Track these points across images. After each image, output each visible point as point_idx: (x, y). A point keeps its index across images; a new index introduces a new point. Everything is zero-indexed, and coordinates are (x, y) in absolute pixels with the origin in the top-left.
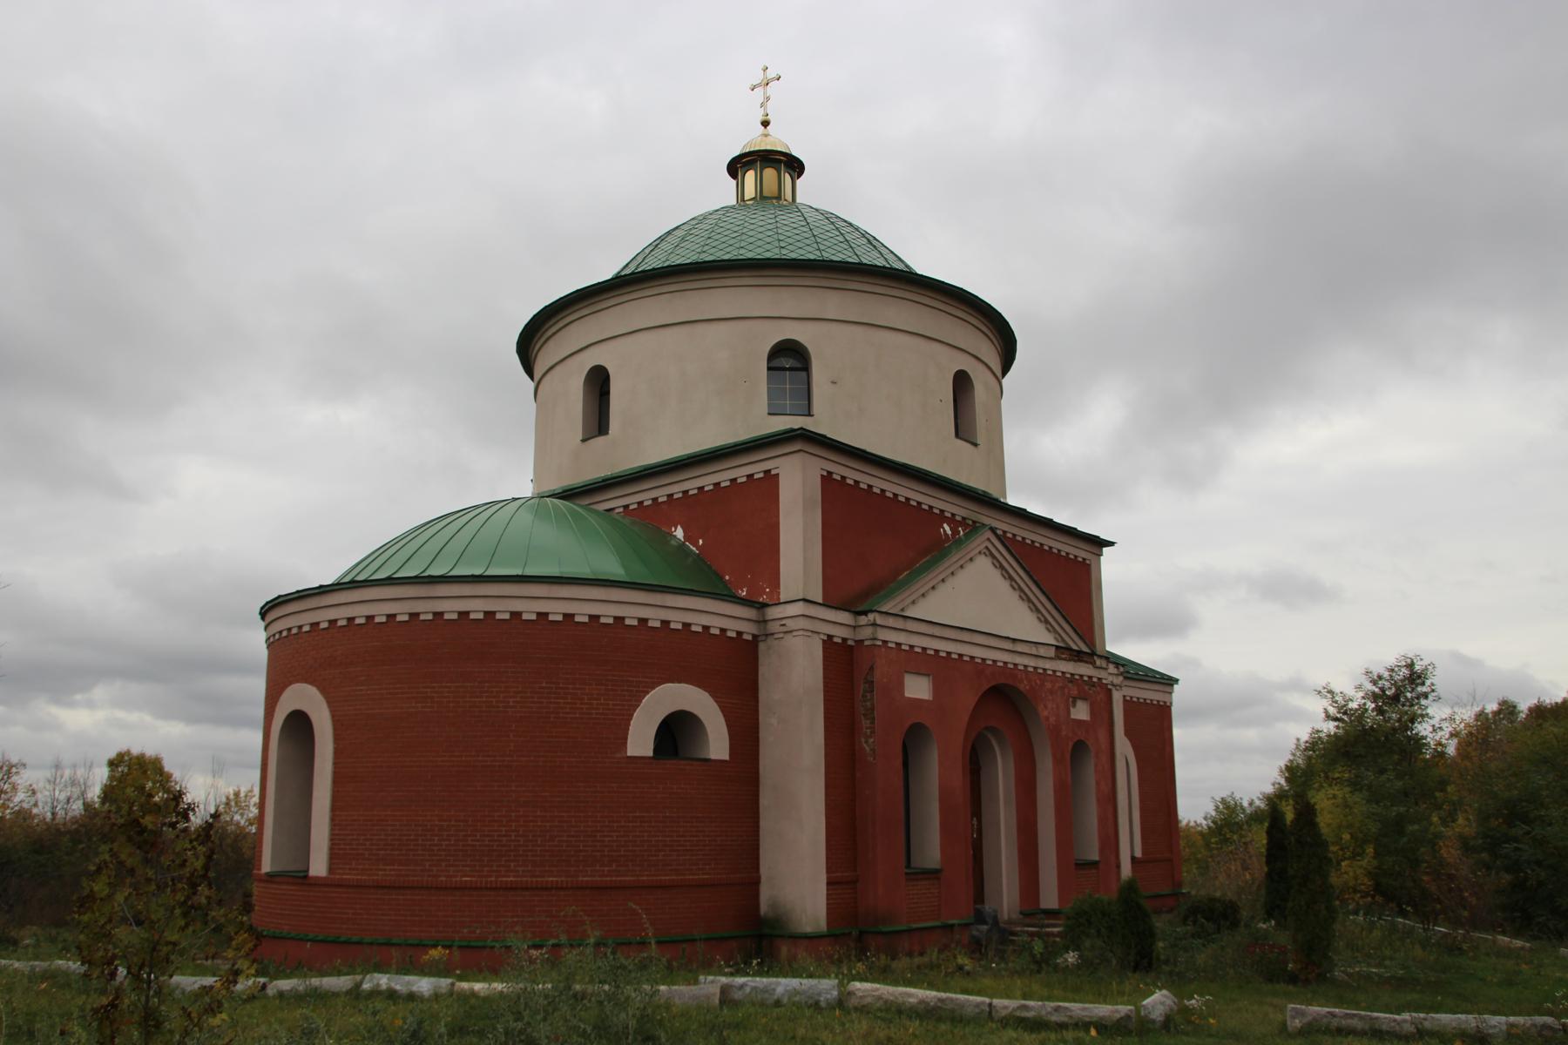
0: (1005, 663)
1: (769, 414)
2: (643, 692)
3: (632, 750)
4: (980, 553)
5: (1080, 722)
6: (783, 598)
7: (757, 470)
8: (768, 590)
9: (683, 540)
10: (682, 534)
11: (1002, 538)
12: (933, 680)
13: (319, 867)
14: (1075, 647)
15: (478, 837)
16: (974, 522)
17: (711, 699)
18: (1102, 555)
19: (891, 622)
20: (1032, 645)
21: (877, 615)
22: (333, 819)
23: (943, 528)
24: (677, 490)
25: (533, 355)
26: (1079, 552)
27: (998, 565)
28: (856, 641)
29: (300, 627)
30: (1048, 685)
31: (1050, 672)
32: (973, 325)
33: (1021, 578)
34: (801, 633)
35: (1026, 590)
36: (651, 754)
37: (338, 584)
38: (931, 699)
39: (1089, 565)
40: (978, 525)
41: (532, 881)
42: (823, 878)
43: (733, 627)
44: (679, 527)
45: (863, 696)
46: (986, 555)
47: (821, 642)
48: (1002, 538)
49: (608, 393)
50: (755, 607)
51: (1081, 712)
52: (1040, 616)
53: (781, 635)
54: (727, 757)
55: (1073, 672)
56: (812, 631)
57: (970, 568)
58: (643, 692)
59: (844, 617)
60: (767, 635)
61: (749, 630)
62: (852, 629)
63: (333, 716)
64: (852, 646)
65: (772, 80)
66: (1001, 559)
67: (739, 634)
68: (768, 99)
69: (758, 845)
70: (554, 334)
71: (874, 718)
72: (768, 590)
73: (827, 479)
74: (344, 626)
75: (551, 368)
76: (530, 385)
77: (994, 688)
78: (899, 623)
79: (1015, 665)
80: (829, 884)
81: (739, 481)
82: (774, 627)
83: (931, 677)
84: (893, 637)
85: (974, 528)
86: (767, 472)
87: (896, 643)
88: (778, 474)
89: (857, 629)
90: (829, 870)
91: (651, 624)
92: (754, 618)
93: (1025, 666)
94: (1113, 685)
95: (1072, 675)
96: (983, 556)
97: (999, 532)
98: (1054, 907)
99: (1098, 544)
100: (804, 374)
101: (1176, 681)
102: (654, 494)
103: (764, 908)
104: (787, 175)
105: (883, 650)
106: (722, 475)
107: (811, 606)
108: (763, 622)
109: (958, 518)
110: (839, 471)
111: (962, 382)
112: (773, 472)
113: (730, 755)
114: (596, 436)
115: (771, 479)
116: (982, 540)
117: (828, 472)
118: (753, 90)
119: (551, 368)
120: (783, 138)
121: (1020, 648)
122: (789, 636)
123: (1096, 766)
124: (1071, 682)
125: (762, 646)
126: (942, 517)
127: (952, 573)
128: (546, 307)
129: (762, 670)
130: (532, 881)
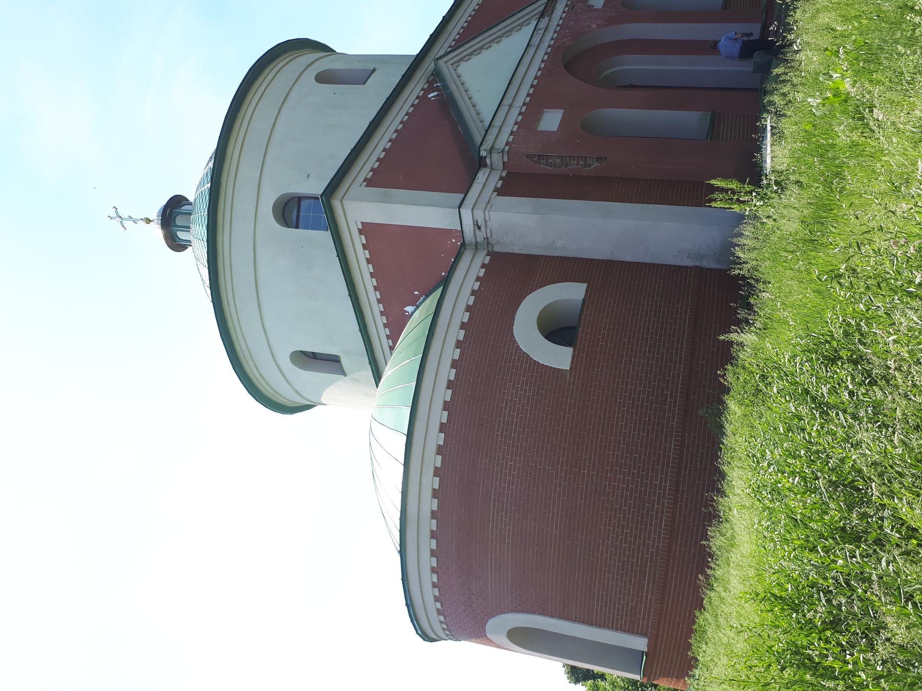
0: (546, 53)
2: (516, 352)
4: (455, 70)
9: (415, 307)
13: (640, 643)
14: (543, 7)
16: (432, 75)
19: (491, 138)
21: (482, 148)
22: (599, 626)
23: (432, 97)
24: (378, 308)
28: (504, 169)
29: (441, 622)
31: (561, 22)
34: (487, 212)
36: (569, 351)
40: (434, 73)
41: (672, 467)
44: (405, 309)
45: (551, 166)
46: (459, 65)
49: (313, 353)
50: (464, 251)
52: (515, 29)
54: (585, 285)
55: (565, 5)
56: (488, 204)
57: (465, 78)
59: (482, 176)
60: (488, 244)
61: (482, 258)
62: (493, 171)
63: (512, 611)
65: (117, 213)
67: (483, 266)
69: (666, 265)
70: (272, 388)
72: (454, 240)
73: (369, 183)
74: (439, 591)
75: (297, 392)
76: (319, 407)
77: (565, 67)
78: (494, 131)
79: (549, 46)
81: (368, 256)
82: (481, 235)
84: (505, 137)
85: (437, 75)
89: (493, 167)
91: (461, 338)
92: (473, 253)
93: (552, 39)
95: (566, 6)
98: (760, 28)
100: (304, 203)
102: (381, 326)
104: (182, 208)
107: (465, 202)
108: (477, 246)
109: (426, 87)
110: (366, 173)
111: (324, 78)
112: (360, 227)
115: (367, 229)
116: (445, 67)
117: (364, 181)
119: (297, 392)
120: (154, 209)
122: (489, 223)
126: (422, 99)
127: (466, 91)
129: (516, 250)
130: (672, 467)
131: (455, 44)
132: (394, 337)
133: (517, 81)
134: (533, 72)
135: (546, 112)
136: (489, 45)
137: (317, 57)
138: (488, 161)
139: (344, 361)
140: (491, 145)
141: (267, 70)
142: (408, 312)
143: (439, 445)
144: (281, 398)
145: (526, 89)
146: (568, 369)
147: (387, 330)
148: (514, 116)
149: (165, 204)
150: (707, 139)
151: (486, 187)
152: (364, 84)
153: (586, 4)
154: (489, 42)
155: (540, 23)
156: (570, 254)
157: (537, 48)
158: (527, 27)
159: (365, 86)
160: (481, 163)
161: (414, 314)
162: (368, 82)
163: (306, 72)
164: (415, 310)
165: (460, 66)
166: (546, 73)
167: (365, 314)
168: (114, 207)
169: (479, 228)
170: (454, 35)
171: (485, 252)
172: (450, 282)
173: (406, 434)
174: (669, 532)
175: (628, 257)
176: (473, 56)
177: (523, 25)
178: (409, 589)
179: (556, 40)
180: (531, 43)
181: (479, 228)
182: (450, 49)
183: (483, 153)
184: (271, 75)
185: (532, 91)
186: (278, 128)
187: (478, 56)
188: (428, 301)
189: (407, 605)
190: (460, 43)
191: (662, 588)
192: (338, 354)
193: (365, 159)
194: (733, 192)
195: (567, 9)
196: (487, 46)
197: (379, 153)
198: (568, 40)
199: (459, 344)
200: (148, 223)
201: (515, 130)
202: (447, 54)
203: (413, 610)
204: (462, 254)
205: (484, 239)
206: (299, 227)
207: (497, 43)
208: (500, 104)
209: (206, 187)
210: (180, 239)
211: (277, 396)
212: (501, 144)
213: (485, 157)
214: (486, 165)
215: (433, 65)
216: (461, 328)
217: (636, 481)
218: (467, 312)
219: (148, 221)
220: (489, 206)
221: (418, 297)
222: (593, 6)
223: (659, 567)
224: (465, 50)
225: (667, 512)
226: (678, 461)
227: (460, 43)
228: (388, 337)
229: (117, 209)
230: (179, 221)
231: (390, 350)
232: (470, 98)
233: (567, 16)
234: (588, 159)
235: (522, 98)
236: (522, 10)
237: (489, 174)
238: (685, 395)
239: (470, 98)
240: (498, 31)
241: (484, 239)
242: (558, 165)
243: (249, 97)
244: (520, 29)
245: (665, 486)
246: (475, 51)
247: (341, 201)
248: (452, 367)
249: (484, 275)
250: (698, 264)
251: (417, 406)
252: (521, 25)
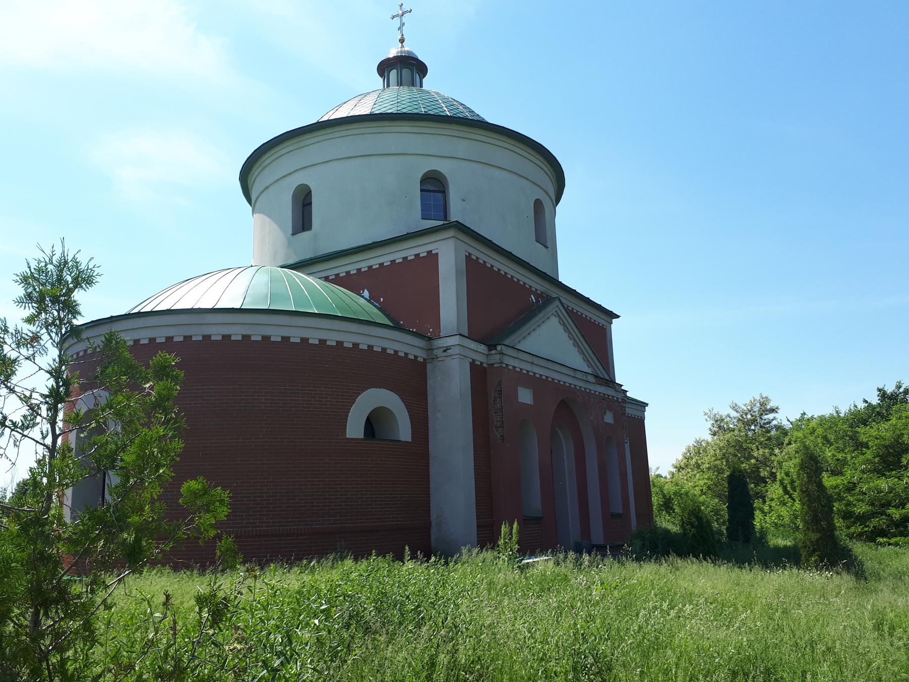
1: (422, 219)
2: (358, 393)
3: (349, 434)
4: (552, 314)
6: (442, 334)
7: (422, 251)
8: (431, 330)
10: (368, 295)
14: (601, 376)
16: (547, 296)
17: (400, 400)
21: (503, 346)
24: (364, 266)
25: (251, 186)
31: (593, 392)
32: (545, 171)
34: (458, 356)
35: (577, 340)
36: (362, 436)
37: (129, 314)
39: (606, 329)
43: (412, 353)
44: (366, 290)
45: (494, 401)
46: (556, 316)
47: (469, 363)
49: (310, 204)
51: (609, 418)
53: (443, 358)
54: (411, 441)
58: (358, 393)
59: (482, 348)
61: (422, 355)
64: (486, 368)
65: (407, 12)
66: (564, 320)
67: (416, 357)
68: (403, 24)
70: (269, 164)
72: (431, 330)
73: (468, 257)
75: (267, 188)
76: (250, 208)
80: (478, 526)
82: (439, 352)
83: (532, 390)
84: (511, 362)
85: (547, 300)
86: (429, 252)
87: (513, 367)
88: (438, 253)
89: (489, 356)
92: (425, 348)
96: (554, 316)
99: (613, 316)
100: (440, 195)
101: (647, 404)
104: (417, 74)
106: (396, 254)
108: (430, 350)
109: (539, 292)
110: (475, 254)
111: (538, 204)
114: (301, 232)
115: (432, 257)
117: (469, 253)
118: (392, 19)
119: (267, 188)
121: (579, 375)
125: (429, 366)
126: (529, 291)
128: (264, 144)
129: (430, 382)
132: (337, 280)
133: (550, 365)
134: (557, 377)
135: (531, 391)
137: (551, 195)
138: (494, 352)
139: (306, 235)
140: (506, 353)
141: (541, 159)
142: (363, 293)
143: (270, 337)
144: (258, 171)
145: (545, 373)
146: (347, 437)
147: (344, 274)
148: (526, 367)
149: (419, 59)
150: (524, 516)
152: (536, 241)
154: (587, 359)
155: (591, 376)
156: (430, 425)
157: (574, 377)
159: (535, 241)
160: (492, 347)
161: (362, 298)
162: (538, 244)
163: (542, 190)
164: (366, 299)
166: (556, 386)
167: (358, 255)
168: (411, 10)
169: (445, 351)
170: (576, 308)
171: (426, 357)
172: (402, 332)
173: (270, 308)
175: (433, 471)
176: (563, 327)
177: (587, 362)
178: (129, 318)
179: (580, 390)
180: (577, 371)
181: (445, 351)
182: (566, 306)
183: (499, 348)
184: (540, 164)
185: (544, 378)
186: (497, 172)
187: (559, 323)
188: (376, 310)
189: (112, 317)
190: (571, 313)
192: (313, 229)
193: (484, 252)
194: (510, 539)
195: (602, 395)
196: (571, 337)
197: (490, 262)
198: (581, 399)
199: (356, 345)
200: (400, 41)
201: (517, 369)
203: (103, 323)
204: (422, 339)
205: (437, 356)
206: (423, 193)
207: (574, 344)
208: (533, 355)
209: (445, 108)
210: (390, 72)
211: (260, 168)
212: (508, 361)
213: (497, 350)
214: (490, 350)
215: (554, 296)
216: (369, 346)
219: (402, 41)
220: (462, 357)
221: (378, 301)
222: (605, 414)
224: (567, 320)
227: (571, 313)
228: (337, 275)
229: (410, 12)
230: (406, 72)
231: (325, 277)
232: (534, 330)
234: (502, 429)
235: (539, 371)
236: (598, 360)
237: (484, 354)
239: (534, 330)
240: (582, 343)
241: (437, 356)
242: (495, 406)
243: (521, 146)
244: (584, 360)
245: (262, 527)
246: (567, 328)
247: (453, 237)
248: (337, 342)
249: (409, 359)
250: (433, 524)
251: (305, 316)
252: (588, 361)
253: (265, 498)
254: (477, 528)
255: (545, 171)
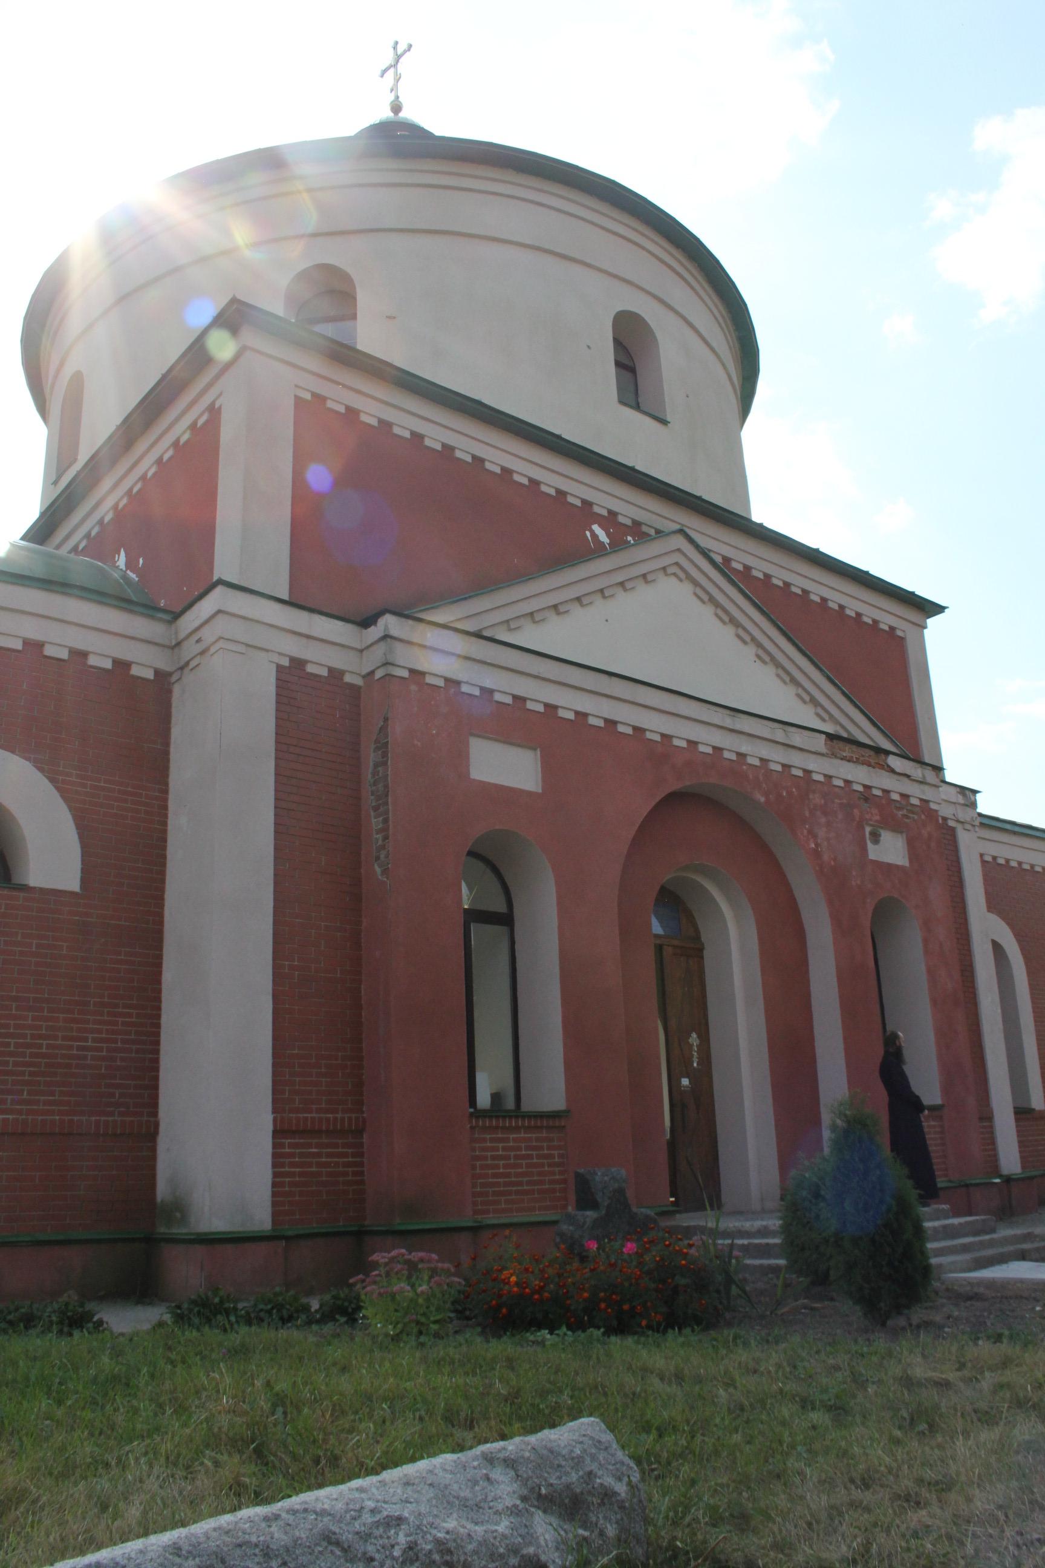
5: (888, 869)
11: (724, 567)
12: (542, 757)
15: (25, 1096)
18: (925, 627)
20: (776, 725)
26: (886, 615)
27: (705, 598)
30: (816, 799)
32: (650, 252)
33: (732, 601)
38: (540, 791)
39: (902, 639)
42: (266, 1121)
47: (274, 668)
48: (724, 567)
50: (160, 620)
52: (800, 691)
56: (247, 645)
57: (644, 594)
60: (182, 668)
64: (360, 687)
69: (156, 1061)
71: (387, 812)
73: (296, 397)
80: (279, 1133)
83: (538, 752)
90: (278, 1104)
94: (958, 821)
97: (718, 559)
99: (929, 609)
103: (162, 1190)
105: (413, 688)
113: (84, 881)
123: (926, 941)
124: (866, 800)
126: (587, 511)
131: (735, 570)
136: (748, 638)
151: (304, 641)
153: (882, 828)
158: (815, 716)
165: (678, 582)
174: (294, 1128)
184: (622, 230)
187: (695, 599)
191: (331, 1128)
196: (745, 637)
202: (705, 553)
217: (30, 1057)
218: (70, 652)
223: (42, 1121)
225: (343, 1119)
226: (102, 1132)
233: (837, 790)
238: (57, 1130)
252: (814, 702)
253: (25, 1096)
254: (274, 1137)
255: (650, 252)
